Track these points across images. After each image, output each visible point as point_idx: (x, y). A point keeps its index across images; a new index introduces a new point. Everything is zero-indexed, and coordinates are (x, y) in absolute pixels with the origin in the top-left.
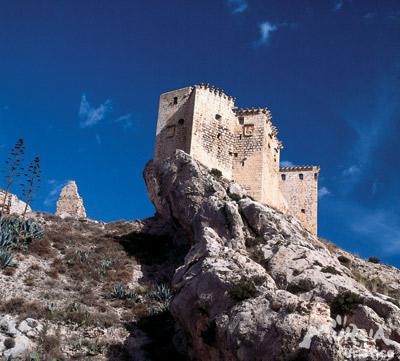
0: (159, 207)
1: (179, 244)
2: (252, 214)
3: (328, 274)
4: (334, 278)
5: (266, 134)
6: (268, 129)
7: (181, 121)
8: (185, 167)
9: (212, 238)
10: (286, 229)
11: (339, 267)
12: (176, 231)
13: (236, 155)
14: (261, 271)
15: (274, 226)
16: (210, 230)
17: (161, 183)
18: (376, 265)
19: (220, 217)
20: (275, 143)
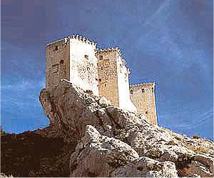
0: (53, 119)
1: (68, 142)
2: (116, 115)
3: (170, 146)
4: (175, 147)
5: (118, 64)
6: (119, 61)
7: (62, 62)
8: (68, 88)
9: (94, 133)
10: (139, 123)
11: (176, 141)
12: (65, 134)
13: (100, 80)
14: (128, 147)
15: (131, 121)
16: (90, 126)
17: (52, 103)
18: (197, 140)
19: (95, 119)
20: (124, 70)
